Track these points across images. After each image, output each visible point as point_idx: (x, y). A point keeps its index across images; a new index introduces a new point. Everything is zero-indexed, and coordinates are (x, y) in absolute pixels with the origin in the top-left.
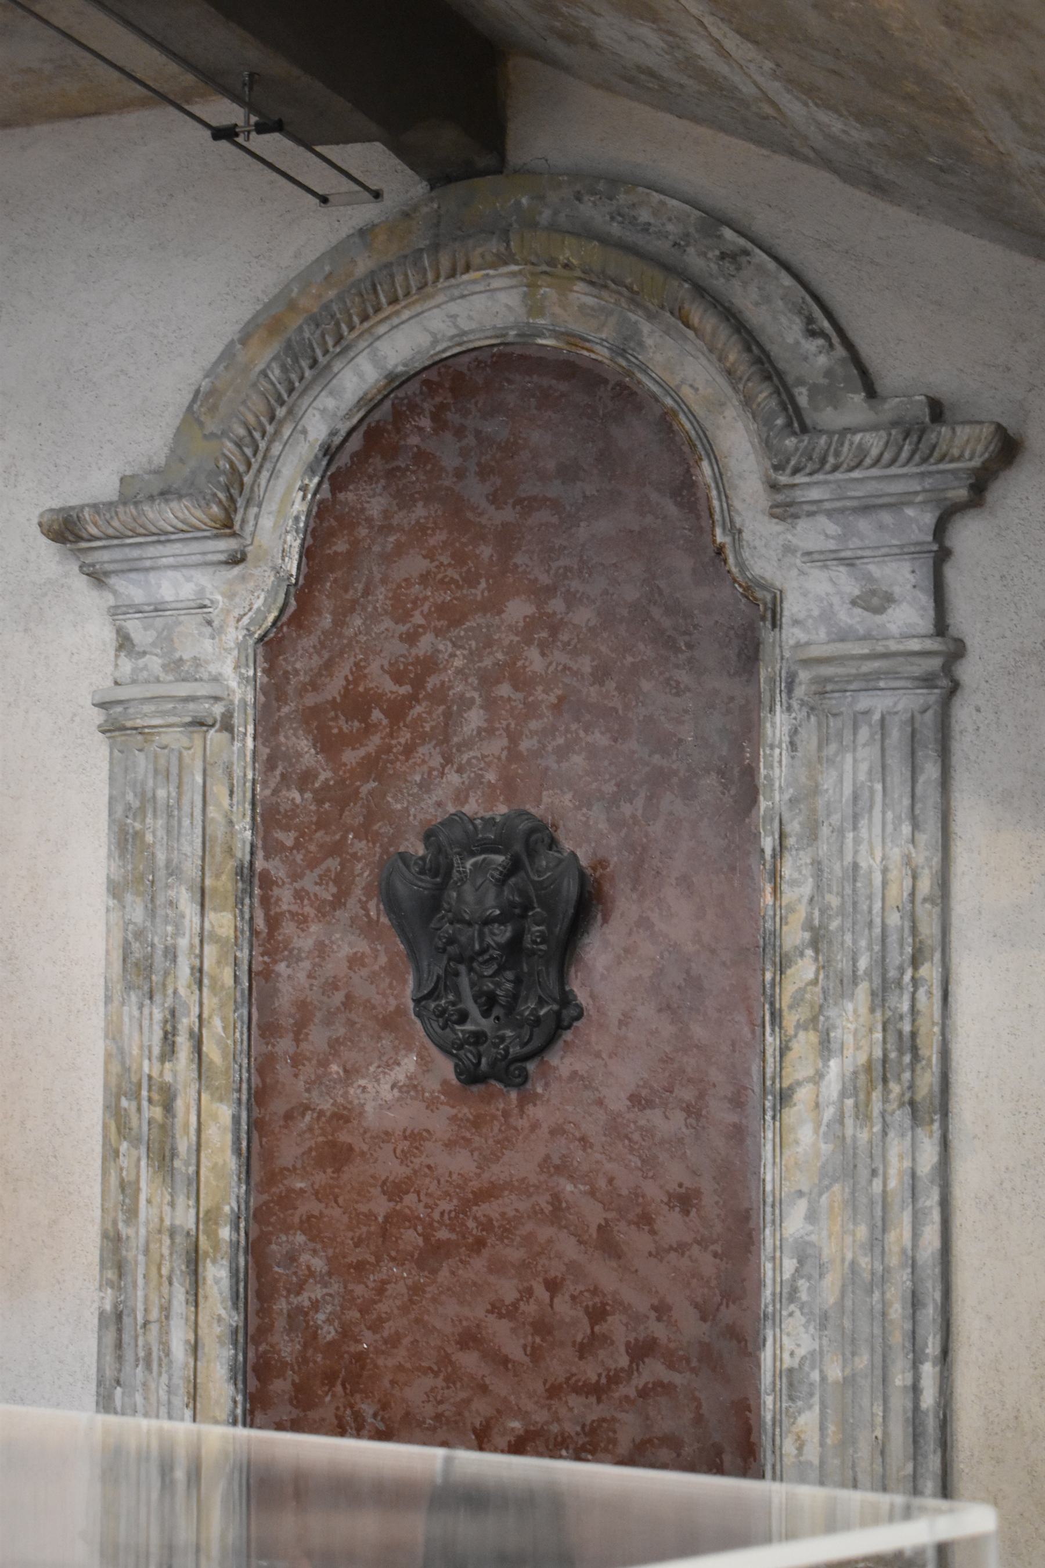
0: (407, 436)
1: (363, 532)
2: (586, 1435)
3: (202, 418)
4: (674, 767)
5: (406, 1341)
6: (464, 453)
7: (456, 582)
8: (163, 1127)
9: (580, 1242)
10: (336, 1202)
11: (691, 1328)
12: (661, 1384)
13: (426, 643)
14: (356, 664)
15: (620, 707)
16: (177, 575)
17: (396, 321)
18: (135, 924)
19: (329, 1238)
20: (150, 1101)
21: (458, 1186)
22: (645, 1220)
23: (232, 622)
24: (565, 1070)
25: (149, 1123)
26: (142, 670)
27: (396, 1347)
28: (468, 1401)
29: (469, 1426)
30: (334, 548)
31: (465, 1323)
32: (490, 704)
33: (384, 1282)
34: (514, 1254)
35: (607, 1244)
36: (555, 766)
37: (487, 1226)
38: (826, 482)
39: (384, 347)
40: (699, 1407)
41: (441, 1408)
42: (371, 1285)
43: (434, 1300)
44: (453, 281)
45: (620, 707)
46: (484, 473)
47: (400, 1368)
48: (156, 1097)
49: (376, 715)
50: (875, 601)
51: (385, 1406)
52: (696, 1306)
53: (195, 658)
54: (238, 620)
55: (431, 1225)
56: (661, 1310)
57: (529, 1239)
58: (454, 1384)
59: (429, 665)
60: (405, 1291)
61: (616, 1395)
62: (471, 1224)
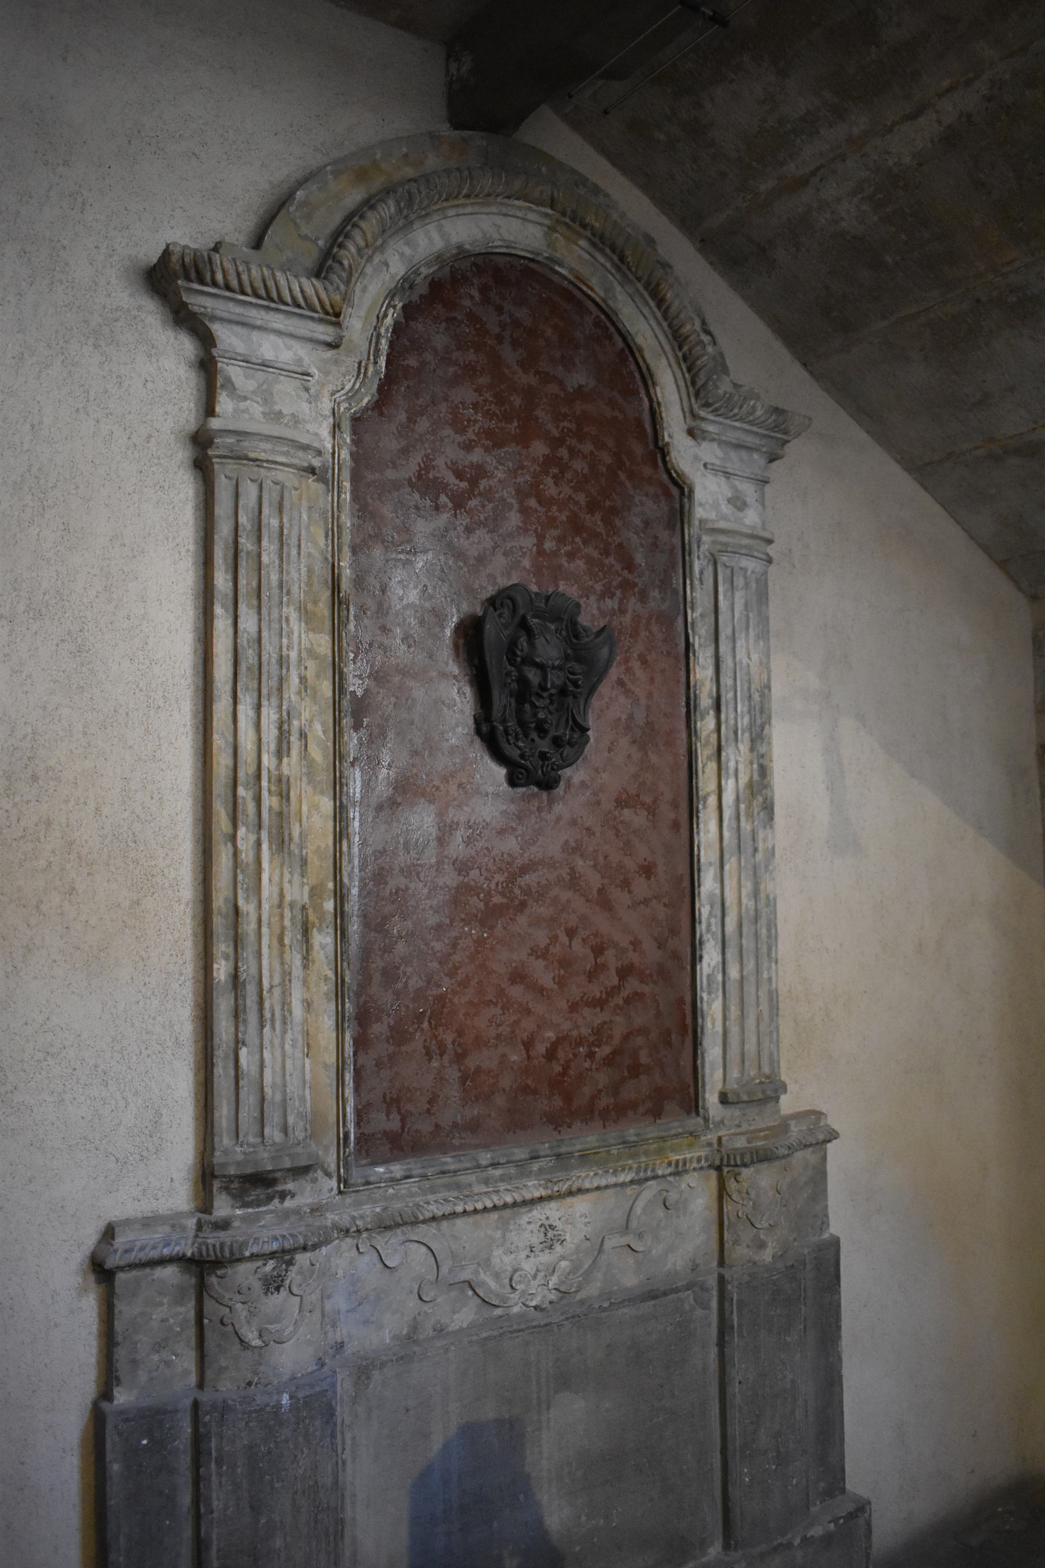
0: (461, 297)
1: (429, 357)
2: (594, 1035)
3: (298, 221)
4: (636, 580)
5: (474, 983)
6: (503, 326)
7: (497, 416)
8: (280, 814)
9: (587, 901)
10: (419, 878)
11: (652, 954)
12: (636, 993)
13: (477, 456)
14: (427, 456)
15: (604, 533)
16: (279, 341)
17: (461, 211)
18: (248, 633)
19: (413, 906)
20: (269, 791)
21: (508, 863)
22: (626, 884)
23: (326, 393)
24: (576, 780)
25: (269, 811)
26: (243, 411)
27: (466, 988)
28: (517, 1023)
29: (519, 1040)
30: (407, 362)
31: (514, 965)
32: (524, 511)
33: (456, 938)
34: (544, 910)
35: (604, 902)
36: (566, 564)
37: (527, 891)
38: (721, 423)
39: (448, 225)
40: (658, 1005)
41: (500, 1029)
42: (447, 941)
43: (492, 949)
44: (507, 201)
45: (604, 533)
46: (515, 344)
47: (470, 1003)
48: (273, 788)
49: (443, 499)
50: (739, 503)
51: (460, 1033)
52: (656, 940)
53: (293, 415)
54: (332, 395)
55: (489, 892)
56: (636, 944)
57: (555, 900)
58: (508, 1010)
59: (480, 472)
60: (471, 944)
61: (612, 1004)
62: (517, 891)
